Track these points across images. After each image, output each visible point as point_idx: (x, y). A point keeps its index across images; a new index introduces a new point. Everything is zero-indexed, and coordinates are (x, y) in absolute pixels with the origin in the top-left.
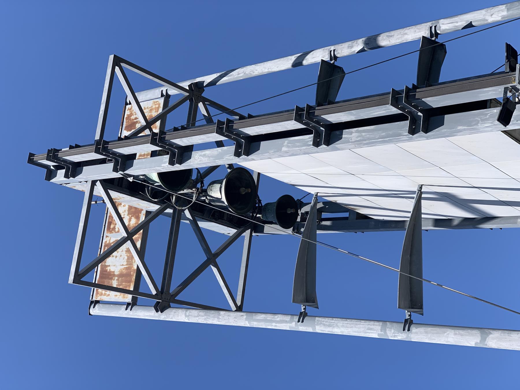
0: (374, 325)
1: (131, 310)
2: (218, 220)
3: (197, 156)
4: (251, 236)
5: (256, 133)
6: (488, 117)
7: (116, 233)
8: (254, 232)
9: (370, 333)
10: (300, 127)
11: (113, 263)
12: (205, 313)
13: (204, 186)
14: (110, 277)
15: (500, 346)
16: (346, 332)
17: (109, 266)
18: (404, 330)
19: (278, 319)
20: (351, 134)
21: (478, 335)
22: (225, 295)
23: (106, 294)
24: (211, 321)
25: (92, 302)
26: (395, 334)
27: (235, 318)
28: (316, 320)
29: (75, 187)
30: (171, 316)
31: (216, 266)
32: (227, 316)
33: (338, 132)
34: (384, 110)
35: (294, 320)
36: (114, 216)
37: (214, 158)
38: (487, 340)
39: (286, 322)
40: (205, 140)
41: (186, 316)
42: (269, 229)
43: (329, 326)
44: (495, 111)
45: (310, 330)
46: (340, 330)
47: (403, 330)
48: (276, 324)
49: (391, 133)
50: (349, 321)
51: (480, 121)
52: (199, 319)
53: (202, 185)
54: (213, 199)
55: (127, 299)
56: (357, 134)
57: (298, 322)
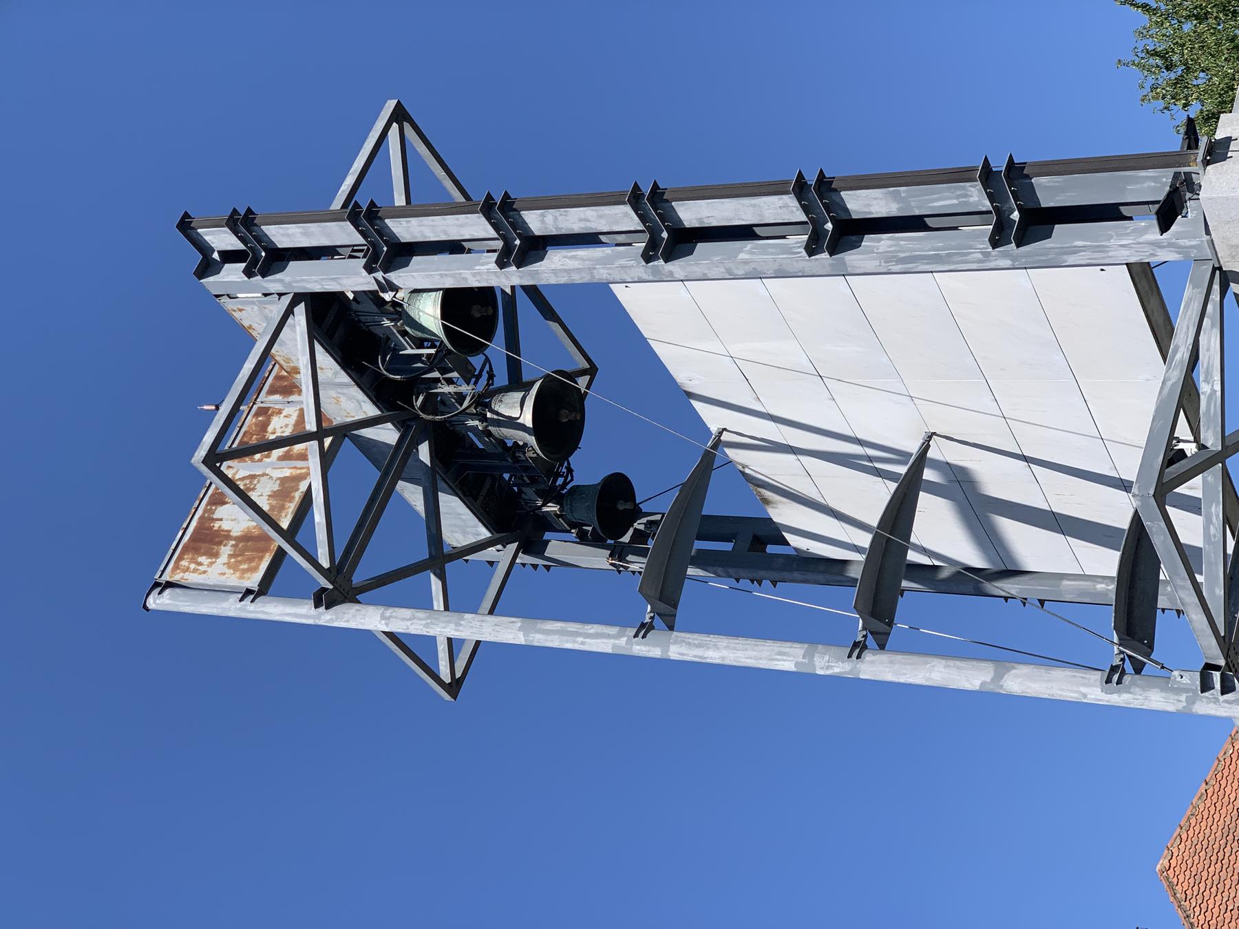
0: (791, 647)
1: (252, 602)
2: (467, 496)
3: (557, 258)
4: (515, 557)
5: (700, 220)
6: (1128, 231)
7: (253, 463)
8: (523, 553)
9: (779, 660)
10: (787, 217)
11: (231, 515)
12: (428, 614)
13: (492, 384)
14: (217, 540)
15: (1026, 690)
16: (731, 658)
17: (221, 520)
18: (850, 656)
19: (592, 631)
20: (879, 242)
21: (991, 669)
22: (438, 645)
23: (198, 570)
24: (439, 629)
25: (157, 585)
26: (830, 664)
27: (495, 625)
28: (673, 636)
29: (241, 310)
30: (346, 617)
31: (442, 577)
32: (478, 621)
33: (854, 238)
34: (958, 197)
35: (626, 633)
36: (305, 383)
37: (594, 263)
38: (1004, 679)
39: (609, 636)
40: (588, 224)
41: (383, 617)
42: (560, 548)
43: (699, 646)
44: (1143, 224)
45: (656, 652)
46: (720, 654)
47: (848, 657)
48: (584, 640)
49: (953, 243)
50: (741, 641)
51: (1115, 237)
52: (412, 624)
53: (490, 382)
54: (500, 418)
55: (249, 581)
56: (891, 242)
57: (634, 637)
